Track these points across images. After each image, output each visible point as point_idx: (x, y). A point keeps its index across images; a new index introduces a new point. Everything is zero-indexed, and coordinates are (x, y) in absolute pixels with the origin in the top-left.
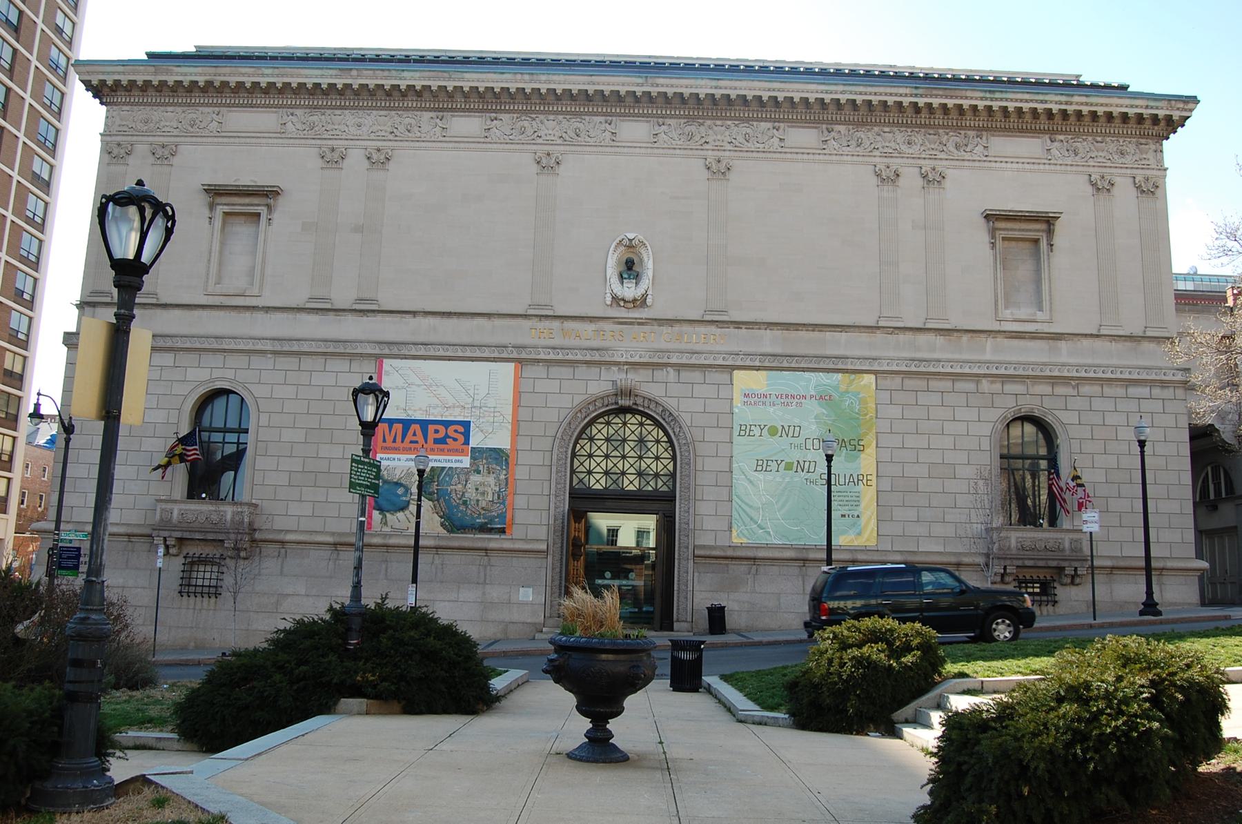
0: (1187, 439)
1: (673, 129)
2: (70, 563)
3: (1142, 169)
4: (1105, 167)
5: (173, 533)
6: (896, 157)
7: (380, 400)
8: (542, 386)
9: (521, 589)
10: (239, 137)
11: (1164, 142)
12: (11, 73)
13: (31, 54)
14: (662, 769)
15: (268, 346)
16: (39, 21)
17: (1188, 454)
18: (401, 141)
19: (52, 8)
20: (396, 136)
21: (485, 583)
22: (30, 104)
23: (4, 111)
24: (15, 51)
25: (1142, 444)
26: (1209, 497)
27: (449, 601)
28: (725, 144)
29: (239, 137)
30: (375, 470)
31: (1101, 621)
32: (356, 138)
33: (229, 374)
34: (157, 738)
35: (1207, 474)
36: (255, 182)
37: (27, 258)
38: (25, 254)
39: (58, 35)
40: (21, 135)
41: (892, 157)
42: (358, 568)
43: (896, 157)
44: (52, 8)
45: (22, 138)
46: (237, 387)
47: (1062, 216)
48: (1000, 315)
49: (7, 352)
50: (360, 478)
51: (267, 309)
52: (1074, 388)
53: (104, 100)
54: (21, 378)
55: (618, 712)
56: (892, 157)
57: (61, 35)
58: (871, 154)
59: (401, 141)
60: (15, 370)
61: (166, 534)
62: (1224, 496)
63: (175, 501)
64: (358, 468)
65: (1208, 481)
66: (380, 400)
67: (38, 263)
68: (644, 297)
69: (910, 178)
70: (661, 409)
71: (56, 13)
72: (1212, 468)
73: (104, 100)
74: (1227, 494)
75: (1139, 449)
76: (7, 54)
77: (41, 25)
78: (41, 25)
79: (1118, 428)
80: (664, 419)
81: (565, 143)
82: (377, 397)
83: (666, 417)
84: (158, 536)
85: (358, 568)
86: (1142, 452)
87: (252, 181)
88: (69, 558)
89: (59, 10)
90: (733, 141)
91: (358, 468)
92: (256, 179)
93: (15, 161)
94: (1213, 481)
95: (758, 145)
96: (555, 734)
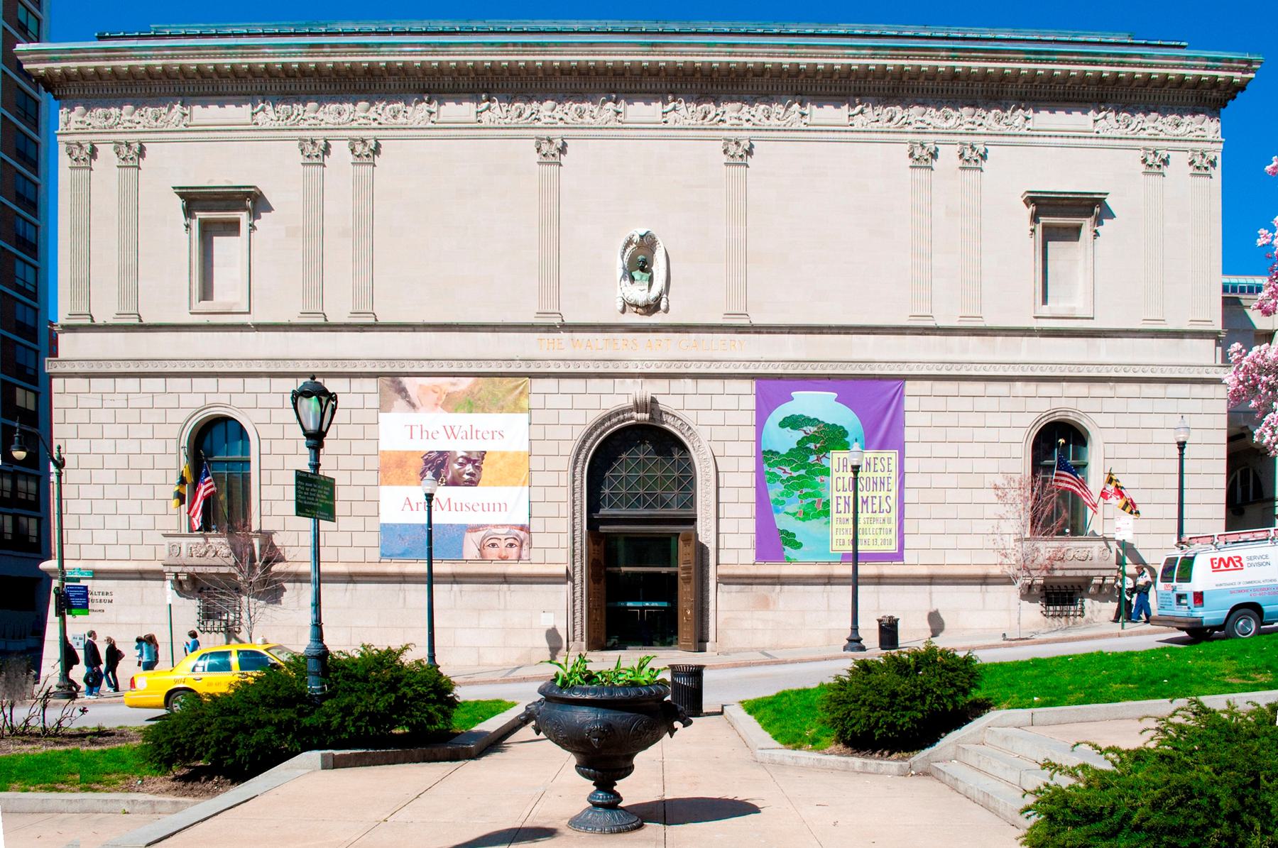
0: (1225, 441)
1: (685, 112)
3: (1197, 141)
5: (172, 567)
6: (931, 133)
7: (324, 404)
11: (1222, 110)
15: (264, 368)
20: (380, 124)
25: (1182, 445)
28: (744, 122)
31: (1129, 631)
33: (224, 399)
35: (1236, 476)
36: (231, 182)
37: (24, 288)
38: (21, 283)
39: (23, 34)
42: (317, 604)
43: (931, 133)
47: (1108, 197)
50: (308, 498)
51: (259, 327)
52: (1111, 389)
55: (627, 770)
56: (925, 133)
57: (26, 33)
58: (902, 130)
61: (178, 569)
62: (66, 584)
63: (183, 536)
64: (305, 487)
66: (324, 404)
67: (36, 294)
68: (658, 300)
71: (17, 6)
72: (1241, 472)
74: (1254, 498)
79: (295, 643)
81: (566, 126)
82: (320, 401)
85: (317, 604)
87: (227, 181)
88: (77, 596)
91: (305, 487)
95: (779, 123)
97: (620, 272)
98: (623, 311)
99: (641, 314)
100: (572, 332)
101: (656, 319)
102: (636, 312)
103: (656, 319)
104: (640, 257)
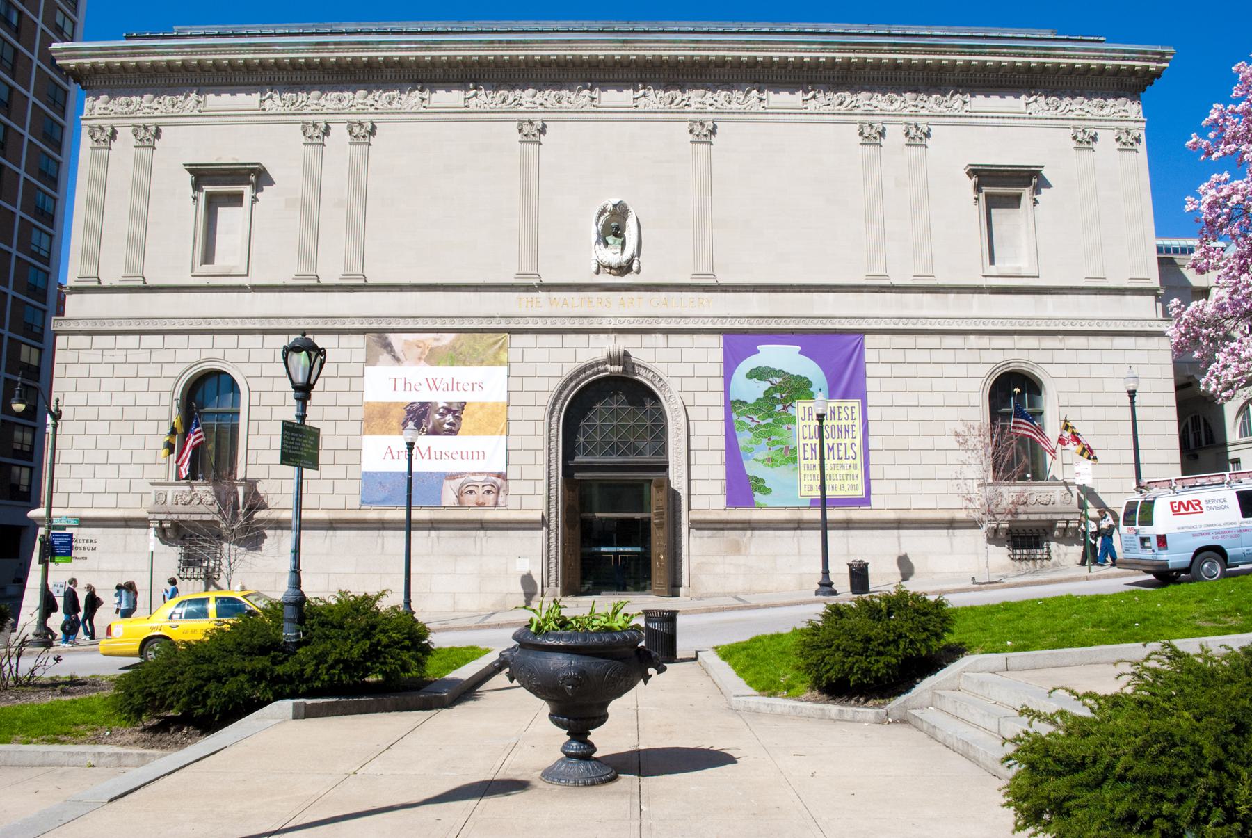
0: (1173, 389)
1: (653, 98)
2: (63, 549)
4: (1085, 120)
5: (157, 515)
7: (313, 358)
8: (530, 355)
9: (518, 560)
10: (218, 115)
12: (12, 73)
13: (33, 54)
14: (632, 794)
16: (39, 21)
17: (1174, 403)
18: (382, 113)
19: (51, 8)
20: (376, 109)
21: (482, 555)
22: (33, 102)
23: (6, 106)
24: (16, 50)
25: (1132, 394)
26: (1189, 447)
27: (446, 574)
29: (218, 115)
30: (313, 438)
32: (337, 111)
33: (218, 354)
34: (70, 753)
36: (237, 160)
38: (36, 249)
40: (26, 133)
41: (873, 115)
42: (297, 551)
44: (51, 8)
45: (27, 136)
46: (227, 367)
48: (986, 271)
49: (23, 346)
53: (84, 84)
54: (38, 369)
58: (852, 112)
59: (382, 113)
60: (31, 363)
64: (291, 436)
65: (1188, 432)
68: (630, 261)
69: (895, 134)
70: (651, 374)
73: (84, 84)
74: (1207, 443)
75: (1129, 399)
76: (8, 55)
77: (41, 25)
78: (41, 25)
80: (654, 385)
82: (309, 355)
83: (656, 382)
84: (154, 520)
85: (297, 551)
86: (1133, 403)
87: (233, 159)
88: (61, 544)
89: (58, 11)
90: (715, 103)
91: (291, 436)
92: (237, 157)
93: (21, 158)
94: (1193, 430)
96: (513, 741)
97: (594, 238)
98: (598, 272)
99: (614, 275)
100: (549, 291)
101: (629, 279)
102: (610, 273)
103: (629, 279)
104: (613, 224)
